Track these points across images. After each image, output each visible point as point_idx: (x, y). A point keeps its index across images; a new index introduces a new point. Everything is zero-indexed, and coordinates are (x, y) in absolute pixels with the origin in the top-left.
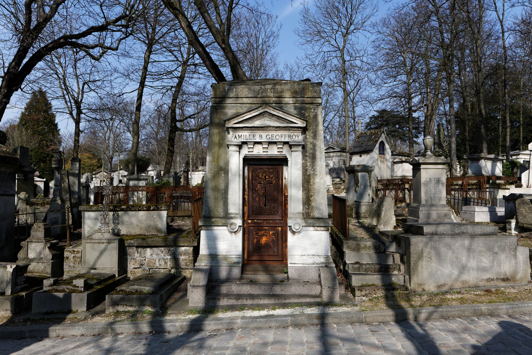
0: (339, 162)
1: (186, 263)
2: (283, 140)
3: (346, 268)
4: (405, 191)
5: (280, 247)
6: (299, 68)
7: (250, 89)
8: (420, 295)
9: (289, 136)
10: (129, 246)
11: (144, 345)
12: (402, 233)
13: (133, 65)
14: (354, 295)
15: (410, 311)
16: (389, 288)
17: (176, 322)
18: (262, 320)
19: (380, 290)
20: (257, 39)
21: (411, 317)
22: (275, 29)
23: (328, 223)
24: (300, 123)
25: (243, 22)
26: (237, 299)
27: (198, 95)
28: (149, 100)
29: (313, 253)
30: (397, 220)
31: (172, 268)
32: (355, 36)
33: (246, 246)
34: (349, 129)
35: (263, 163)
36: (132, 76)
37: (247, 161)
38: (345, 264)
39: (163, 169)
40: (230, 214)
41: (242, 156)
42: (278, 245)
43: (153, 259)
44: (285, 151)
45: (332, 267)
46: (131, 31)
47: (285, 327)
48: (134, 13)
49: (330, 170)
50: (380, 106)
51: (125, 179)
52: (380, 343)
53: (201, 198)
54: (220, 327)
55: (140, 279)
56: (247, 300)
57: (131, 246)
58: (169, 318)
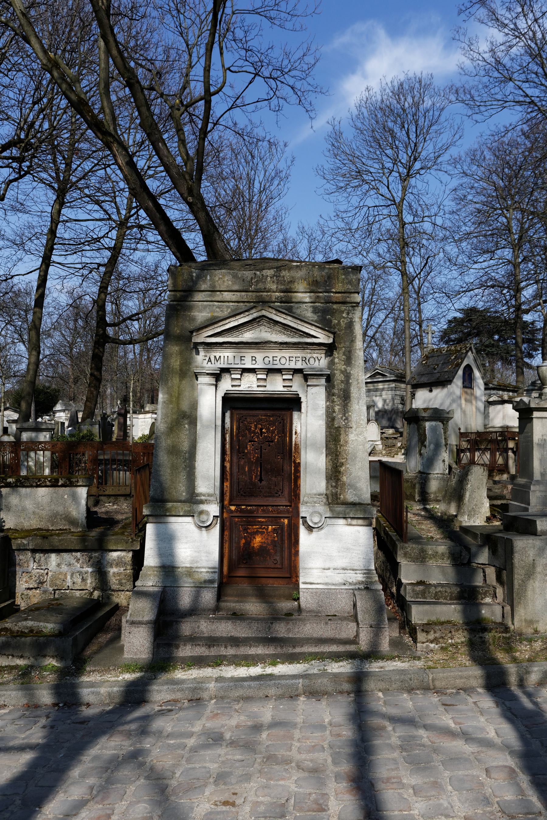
0: (393, 399)
1: (120, 580)
2: (293, 366)
3: (402, 592)
4: (507, 453)
5: (286, 554)
6: (324, 233)
7: (235, 276)
8: (530, 641)
9: (304, 359)
10: (19, 550)
11: (44, 727)
12: (500, 531)
13: (30, 227)
14: (415, 640)
15: (512, 669)
16: (476, 627)
17: (100, 686)
18: (252, 684)
19: (460, 632)
20: (250, 182)
21: (513, 679)
22: (282, 166)
23: (370, 513)
24: (323, 337)
25: (227, 153)
26: (209, 647)
27: (145, 279)
28: (59, 287)
29: (344, 565)
30: (492, 506)
31: (94, 589)
32: (423, 181)
33: (226, 551)
34: (411, 342)
36: (29, 245)
37: (229, 402)
38: (399, 584)
39: (82, 409)
40: (198, 495)
41: (220, 394)
42: (282, 551)
43: (61, 573)
44: (296, 386)
45: (376, 590)
46: (28, 167)
47: (293, 697)
48: (34, 137)
49: (377, 413)
50: (465, 302)
51: (14, 427)
52: (458, 727)
53: (148, 465)
54: (179, 695)
55: (38, 609)
56: (226, 647)
57: (22, 549)
58: (88, 680)
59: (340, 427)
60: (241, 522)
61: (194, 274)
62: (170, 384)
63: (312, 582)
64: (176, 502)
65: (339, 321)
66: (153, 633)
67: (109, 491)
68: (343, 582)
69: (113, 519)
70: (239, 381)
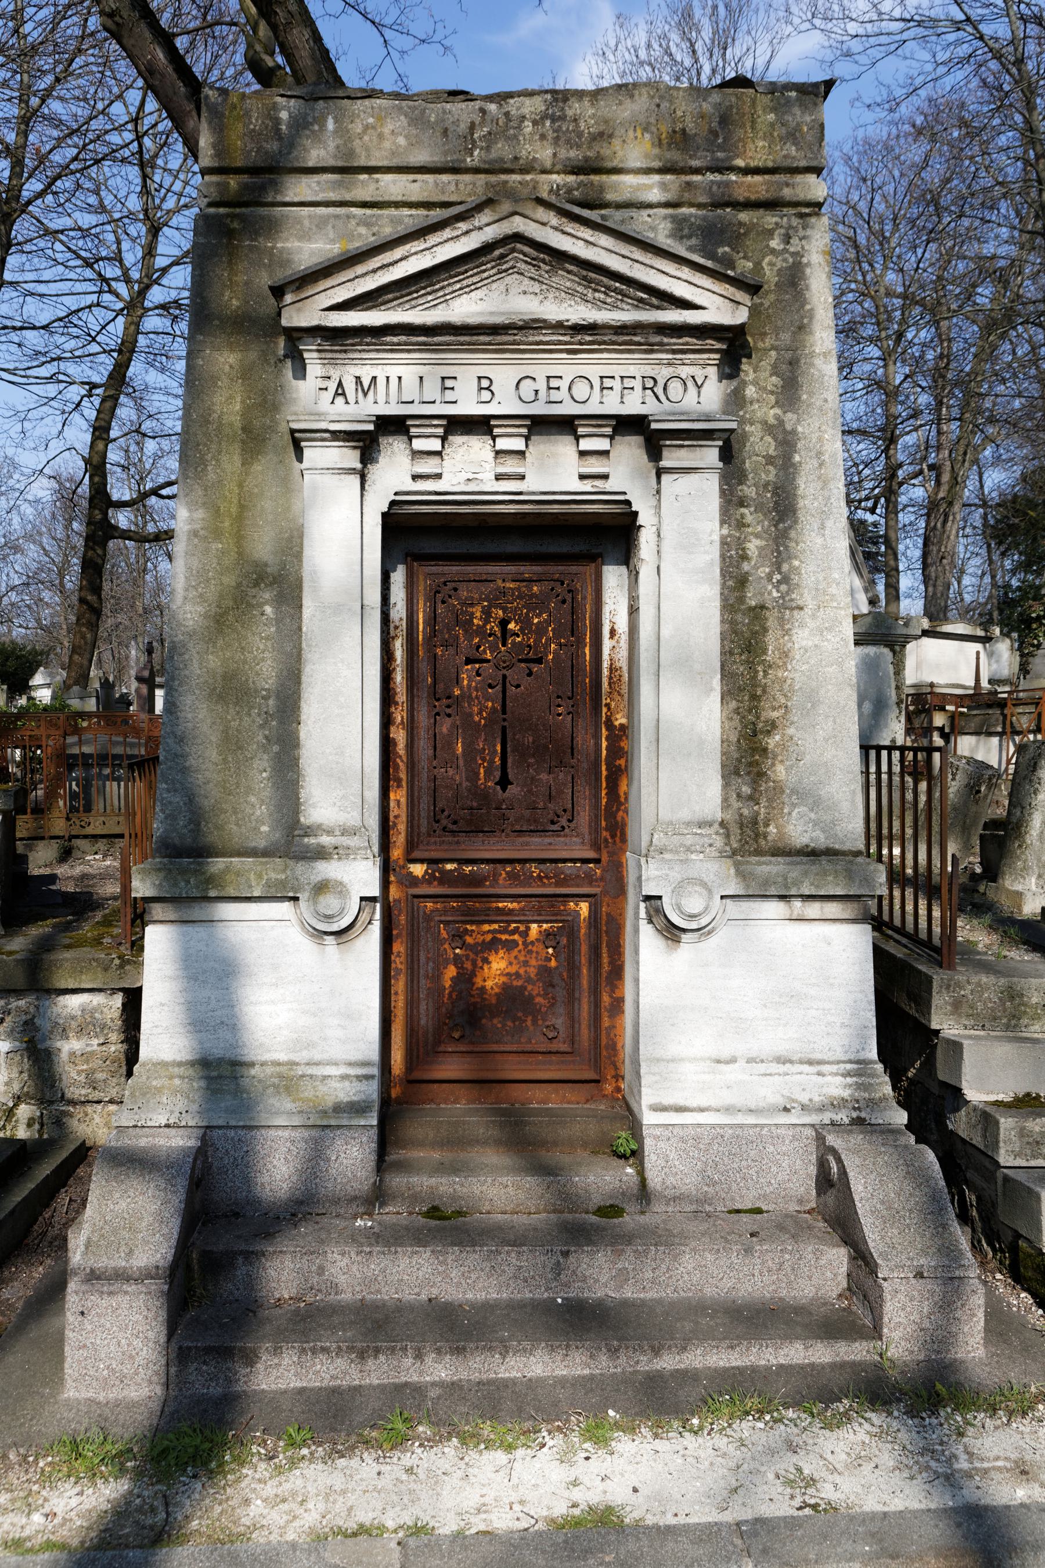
1: (90, 1074)
2: (612, 406)
9: (650, 385)
23: (868, 881)
24: (716, 306)
26: (362, 1355)
29: (782, 1048)
33: (399, 1003)
35: (492, 547)
37: (411, 534)
40: (310, 831)
41: (378, 503)
42: (571, 999)
44: (624, 472)
56: (419, 1356)
59: (763, 607)
60: (445, 912)
61: (284, 115)
62: (212, 476)
63: (682, 1103)
64: (239, 854)
65: (758, 265)
66: (163, 1315)
67: (96, 827)
68: (781, 1102)
69: (90, 894)
70: (436, 460)
